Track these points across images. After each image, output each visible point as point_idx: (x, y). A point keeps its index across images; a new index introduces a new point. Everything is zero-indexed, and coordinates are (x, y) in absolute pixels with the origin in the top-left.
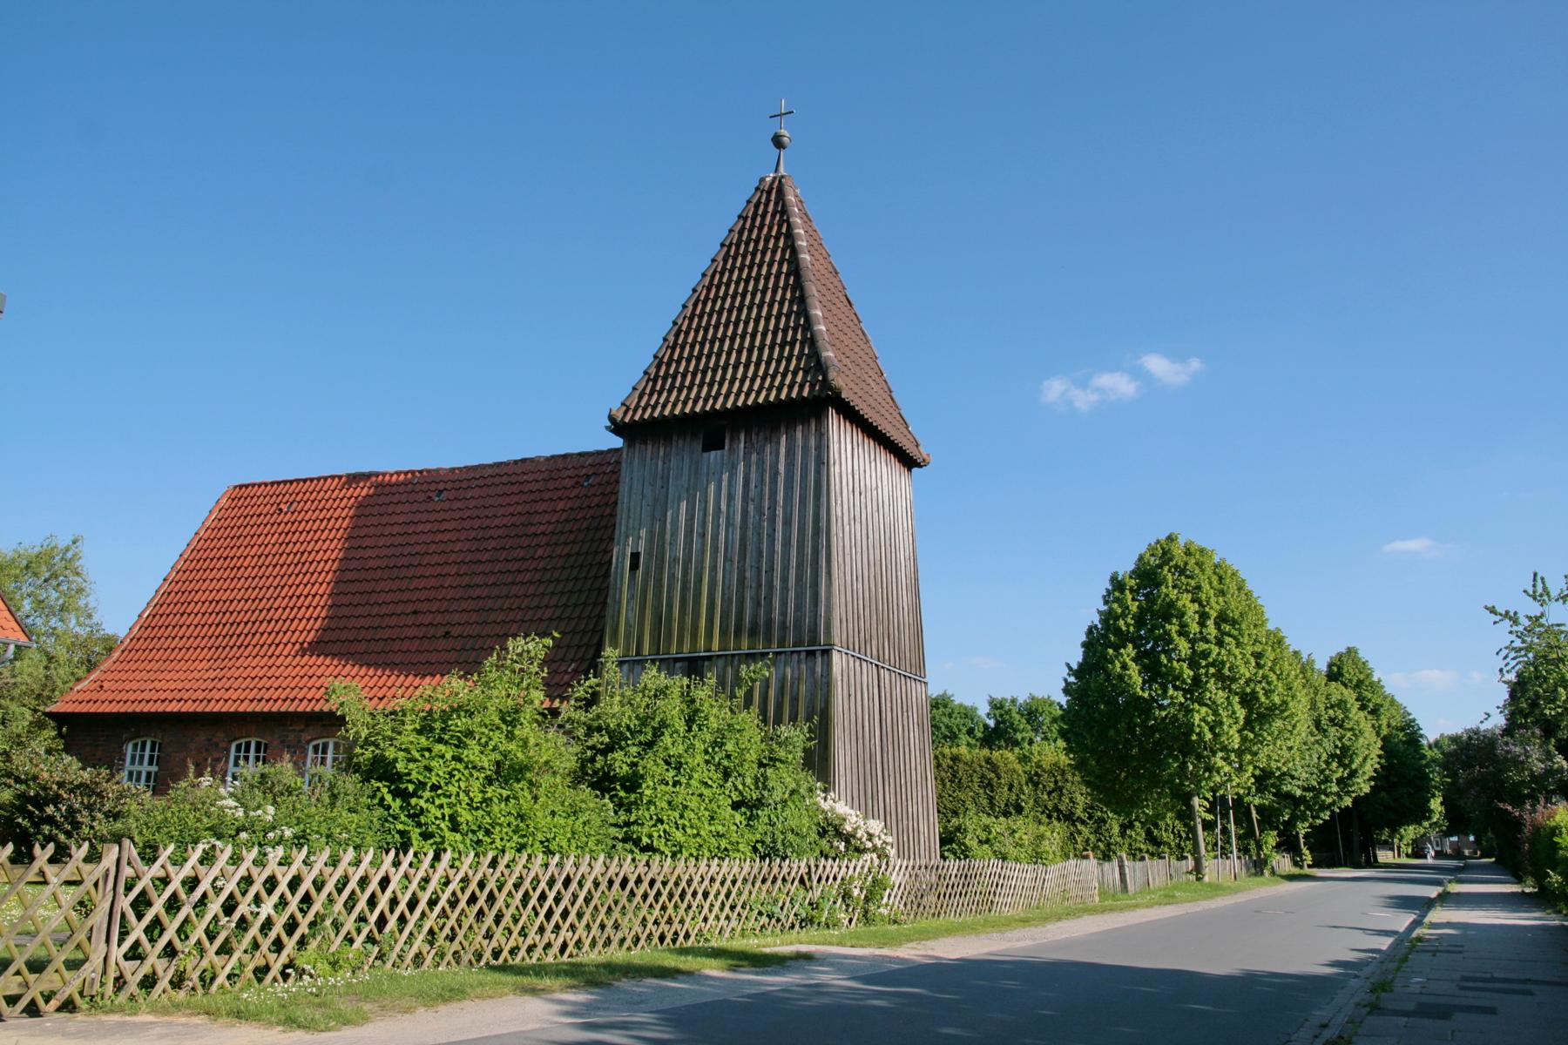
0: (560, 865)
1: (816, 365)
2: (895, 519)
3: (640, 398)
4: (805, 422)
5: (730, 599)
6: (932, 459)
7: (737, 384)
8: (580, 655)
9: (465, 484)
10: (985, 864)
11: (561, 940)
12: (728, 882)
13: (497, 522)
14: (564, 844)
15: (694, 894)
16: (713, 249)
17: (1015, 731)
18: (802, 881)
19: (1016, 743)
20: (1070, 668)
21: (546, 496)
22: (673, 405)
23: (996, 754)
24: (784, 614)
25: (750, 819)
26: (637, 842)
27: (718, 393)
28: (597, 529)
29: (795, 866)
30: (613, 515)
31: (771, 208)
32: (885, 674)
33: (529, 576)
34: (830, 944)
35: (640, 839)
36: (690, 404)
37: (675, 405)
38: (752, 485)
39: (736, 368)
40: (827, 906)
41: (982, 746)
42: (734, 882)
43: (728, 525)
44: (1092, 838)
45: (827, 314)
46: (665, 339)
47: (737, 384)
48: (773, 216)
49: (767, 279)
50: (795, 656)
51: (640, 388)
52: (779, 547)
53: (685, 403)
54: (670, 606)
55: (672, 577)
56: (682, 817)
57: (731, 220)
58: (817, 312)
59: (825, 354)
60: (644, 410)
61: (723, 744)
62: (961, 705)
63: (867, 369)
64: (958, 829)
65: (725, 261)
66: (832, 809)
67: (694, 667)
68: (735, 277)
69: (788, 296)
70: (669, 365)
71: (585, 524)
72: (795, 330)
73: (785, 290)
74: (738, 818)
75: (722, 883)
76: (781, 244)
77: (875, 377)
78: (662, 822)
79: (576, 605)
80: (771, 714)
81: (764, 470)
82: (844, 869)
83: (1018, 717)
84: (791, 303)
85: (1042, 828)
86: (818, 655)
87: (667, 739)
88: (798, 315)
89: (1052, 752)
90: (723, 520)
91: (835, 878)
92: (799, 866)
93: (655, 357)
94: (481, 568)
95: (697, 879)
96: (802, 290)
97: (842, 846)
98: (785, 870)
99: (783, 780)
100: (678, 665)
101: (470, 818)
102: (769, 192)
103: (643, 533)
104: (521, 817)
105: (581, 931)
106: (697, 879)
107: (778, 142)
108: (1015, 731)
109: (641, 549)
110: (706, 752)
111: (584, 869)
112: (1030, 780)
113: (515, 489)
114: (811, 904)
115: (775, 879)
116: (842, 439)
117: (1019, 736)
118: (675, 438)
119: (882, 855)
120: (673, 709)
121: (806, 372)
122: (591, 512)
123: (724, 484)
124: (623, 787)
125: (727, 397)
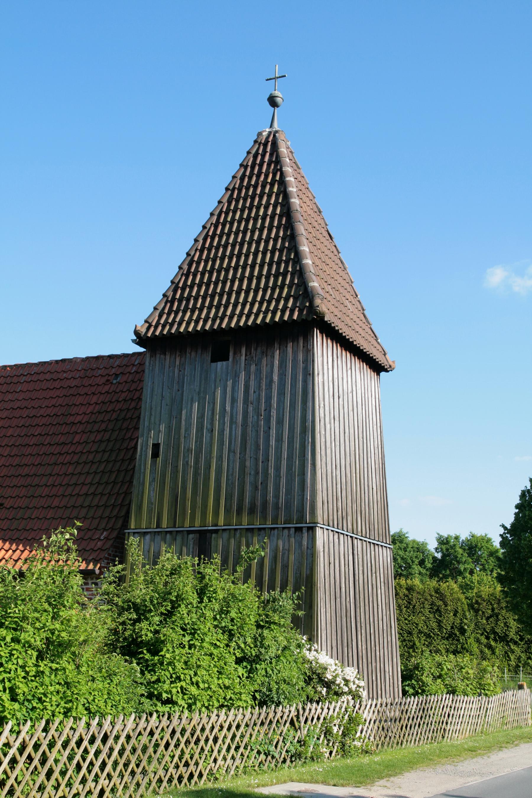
0: (100, 725)
1: (305, 294)
2: (367, 416)
3: (160, 316)
4: (295, 339)
5: (233, 484)
6: (398, 367)
7: (239, 307)
8: (110, 525)
9: (15, 380)
10: (440, 700)
11: (99, 787)
12: (234, 728)
13: (42, 412)
14: (102, 704)
15: (207, 740)
16: (220, 192)
17: (459, 562)
18: (292, 723)
19: (460, 573)
20: (505, 528)
21: (83, 391)
22: (188, 324)
23: (444, 586)
24: (277, 496)
25: (250, 672)
26: (159, 697)
27: (224, 315)
28: (124, 419)
29: (287, 711)
30: (137, 408)
31: (267, 159)
32: (358, 544)
33: (68, 458)
34: (317, 782)
35: (160, 694)
36: (201, 323)
37: (188, 324)
38: (252, 391)
39: (238, 293)
40: (312, 743)
41: (431, 577)
42: (238, 727)
43: (232, 422)
44: (523, 656)
45: (314, 249)
46: (180, 268)
47: (239, 307)
48: (269, 165)
49: (264, 219)
50: (286, 531)
51: (160, 308)
52: (273, 442)
53: (197, 322)
54: (184, 488)
55: (186, 464)
56: (196, 674)
57: (234, 168)
58: (305, 248)
59: (311, 284)
60: (164, 326)
61: (228, 612)
62: (414, 541)
63: (345, 293)
64: (416, 667)
65: (229, 203)
66: (316, 659)
67: (202, 544)
68: (237, 217)
69: (281, 234)
70: (183, 289)
71: (115, 416)
72: (287, 263)
73: (278, 228)
74: (241, 671)
75: (229, 729)
76: (275, 190)
77: (351, 298)
78: (179, 678)
79: (107, 483)
80: (266, 578)
81: (261, 379)
82: (326, 710)
83: (460, 551)
84: (284, 239)
85: (485, 663)
86: (305, 530)
87: (183, 609)
88: (289, 250)
89: (487, 584)
90: (227, 419)
91: (318, 718)
92: (290, 710)
93: (172, 282)
94: (29, 450)
95: (208, 728)
96: (293, 229)
97: (324, 691)
98: (279, 715)
99: (277, 638)
100: (191, 536)
101: (26, 690)
102: (265, 145)
103: (163, 427)
104: (68, 684)
105: (116, 779)
106: (208, 728)
107: (273, 102)
108: (459, 562)
109: (161, 440)
110: (215, 619)
111: (118, 727)
112: (471, 606)
113: (57, 384)
114: (299, 742)
115: (271, 722)
116: (324, 351)
117: (462, 567)
118: (188, 350)
119: (356, 696)
120: (187, 585)
121: (296, 299)
122: (119, 406)
123: (230, 386)
124: (149, 651)
125: (231, 318)
